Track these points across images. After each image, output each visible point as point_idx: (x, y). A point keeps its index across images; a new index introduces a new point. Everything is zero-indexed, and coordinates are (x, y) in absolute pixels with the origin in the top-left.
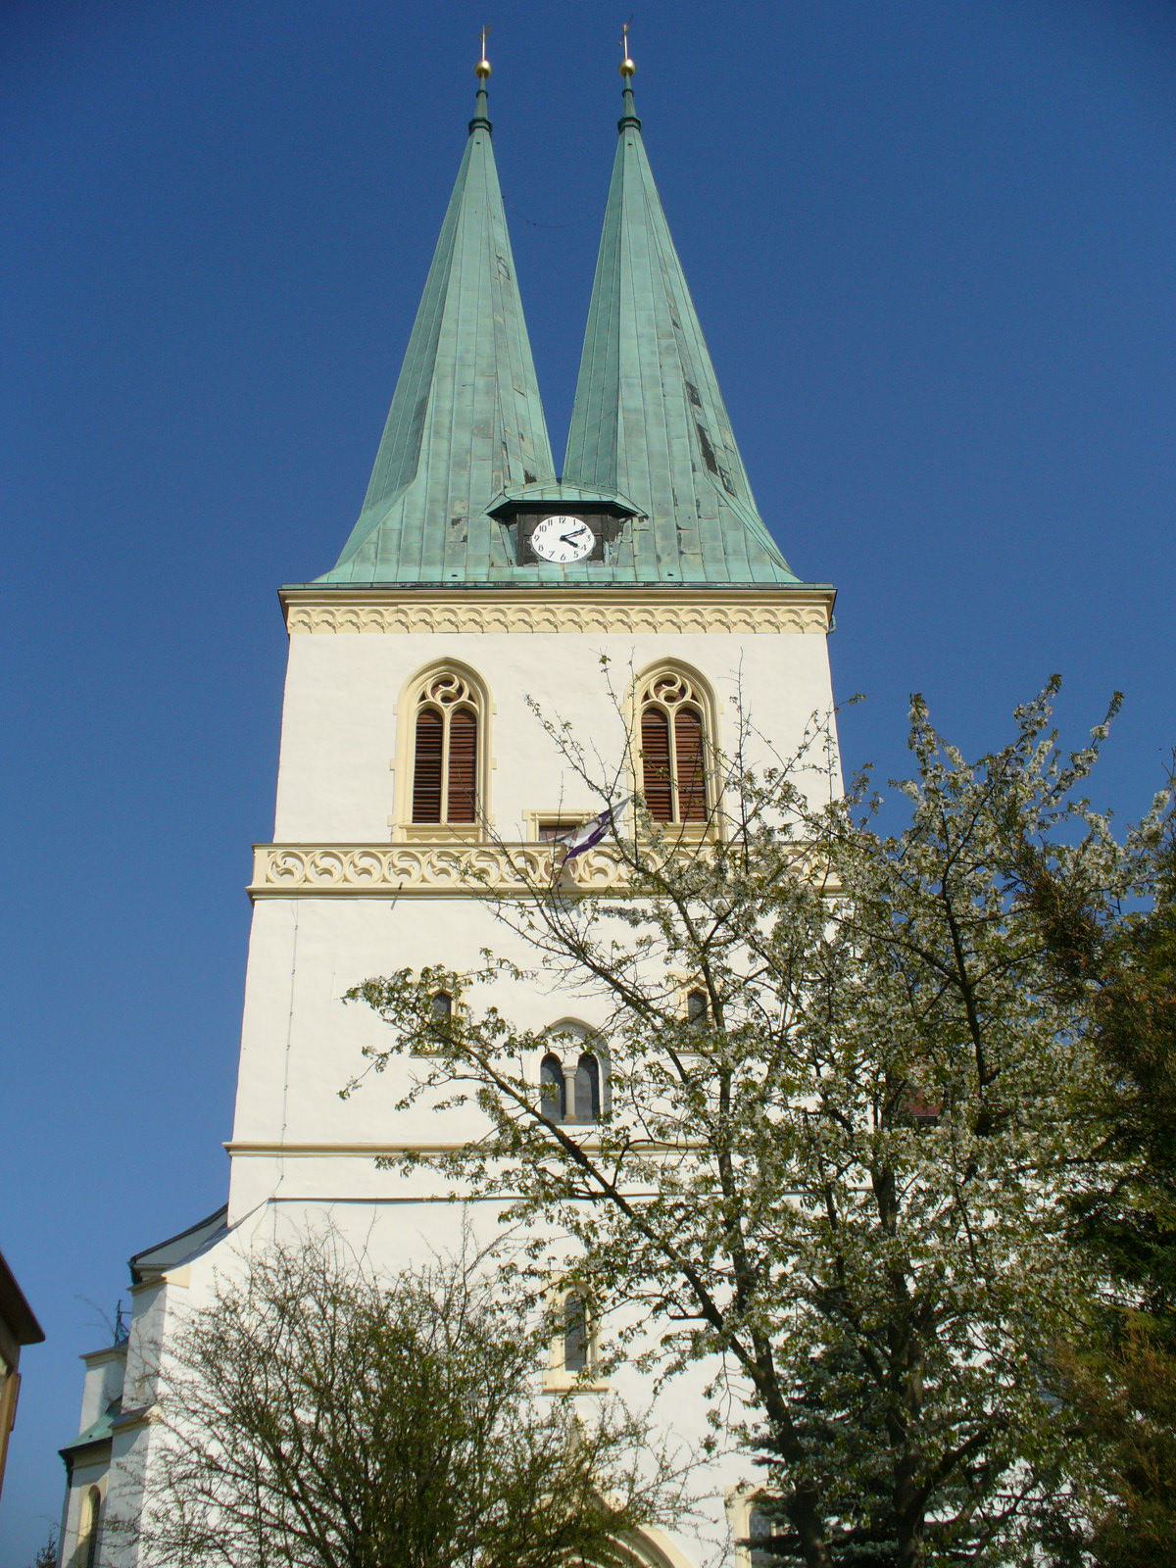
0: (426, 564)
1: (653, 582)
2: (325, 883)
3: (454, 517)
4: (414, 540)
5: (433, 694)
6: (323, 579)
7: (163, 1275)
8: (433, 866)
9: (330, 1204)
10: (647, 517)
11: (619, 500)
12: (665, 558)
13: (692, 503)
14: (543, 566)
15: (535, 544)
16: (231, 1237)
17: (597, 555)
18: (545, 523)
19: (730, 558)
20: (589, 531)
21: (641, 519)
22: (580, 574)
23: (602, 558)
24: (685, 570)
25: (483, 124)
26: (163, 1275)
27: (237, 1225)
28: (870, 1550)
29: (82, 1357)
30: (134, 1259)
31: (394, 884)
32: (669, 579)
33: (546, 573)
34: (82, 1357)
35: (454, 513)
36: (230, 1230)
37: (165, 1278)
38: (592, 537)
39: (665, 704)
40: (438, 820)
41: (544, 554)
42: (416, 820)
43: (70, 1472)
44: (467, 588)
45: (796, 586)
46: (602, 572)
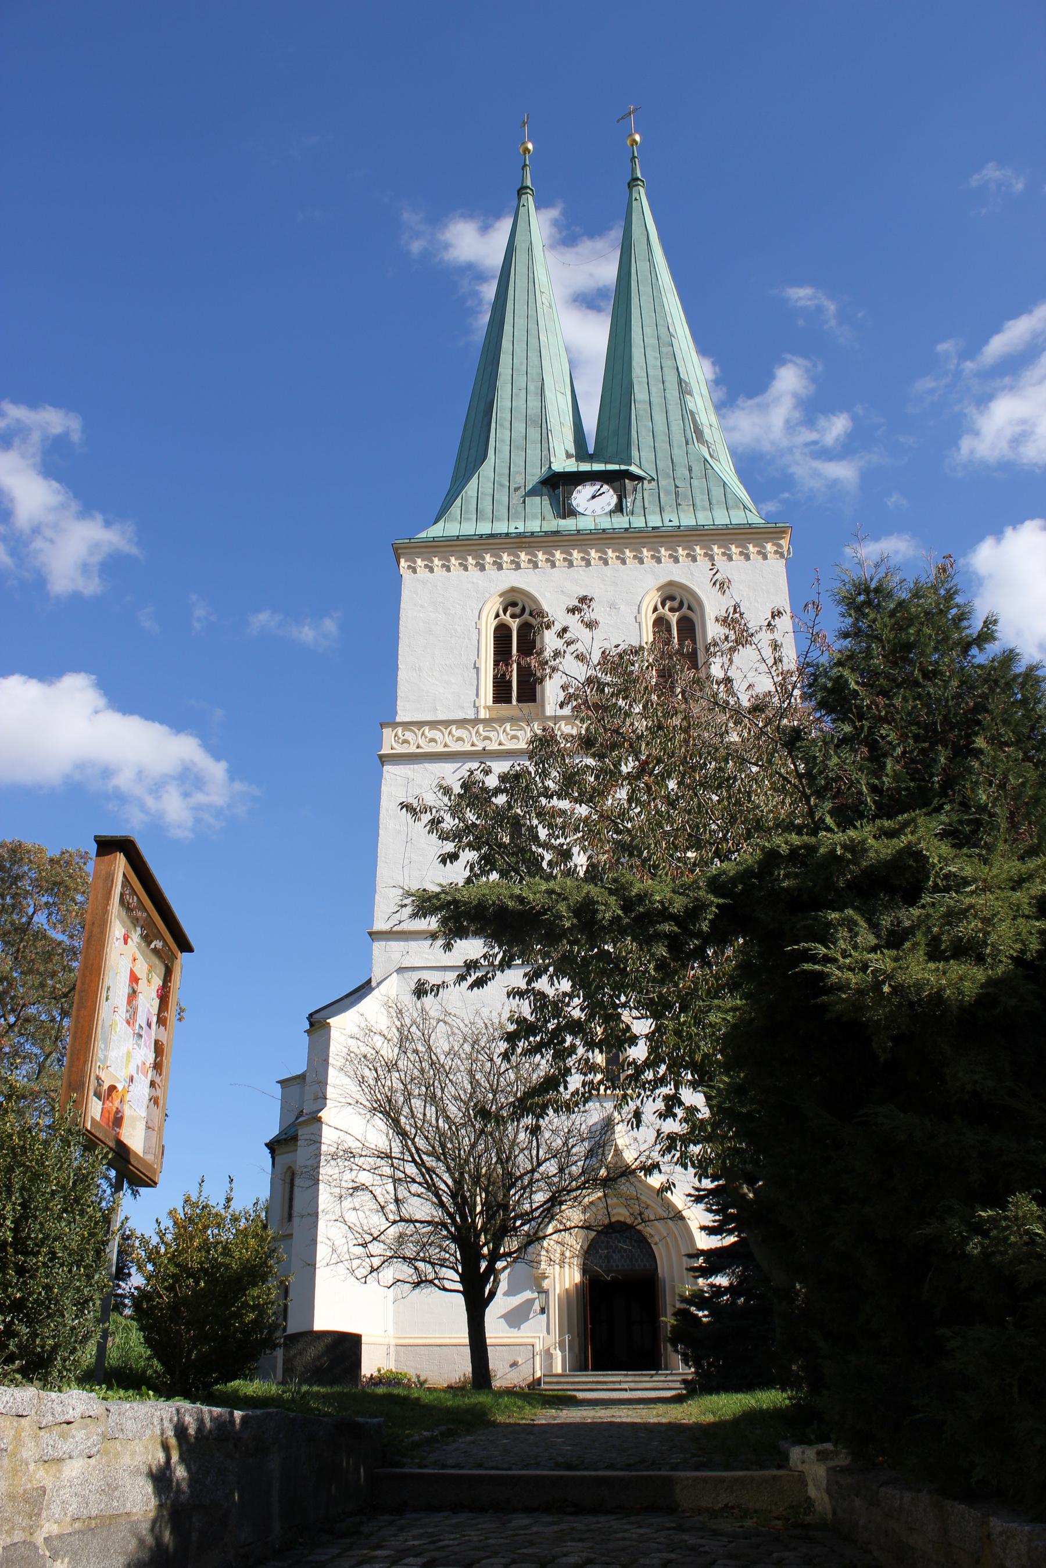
0: (496, 520)
1: (658, 527)
2: (427, 748)
3: (516, 486)
4: (486, 504)
5: (505, 615)
6: (423, 535)
7: (328, 1021)
8: (507, 734)
9: (438, 1348)
10: (653, 479)
11: (634, 469)
12: (667, 509)
13: (670, 477)
14: (580, 518)
15: (574, 503)
16: (375, 992)
17: (619, 508)
18: (579, 488)
19: (715, 507)
20: (611, 490)
21: (650, 482)
22: (605, 523)
23: (621, 511)
24: (682, 515)
25: (529, 191)
26: (328, 1021)
27: (379, 984)
28: (514, 658)
29: (277, 1082)
30: (311, 1015)
31: (479, 748)
32: (671, 524)
33: (584, 523)
34: (277, 1082)
35: (516, 483)
36: (373, 989)
37: (329, 1023)
38: (615, 496)
39: (670, 614)
40: (509, 701)
41: (580, 509)
42: (495, 702)
43: (273, 1158)
44: (526, 537)
45: (762, 526)
46: (620, 522)
